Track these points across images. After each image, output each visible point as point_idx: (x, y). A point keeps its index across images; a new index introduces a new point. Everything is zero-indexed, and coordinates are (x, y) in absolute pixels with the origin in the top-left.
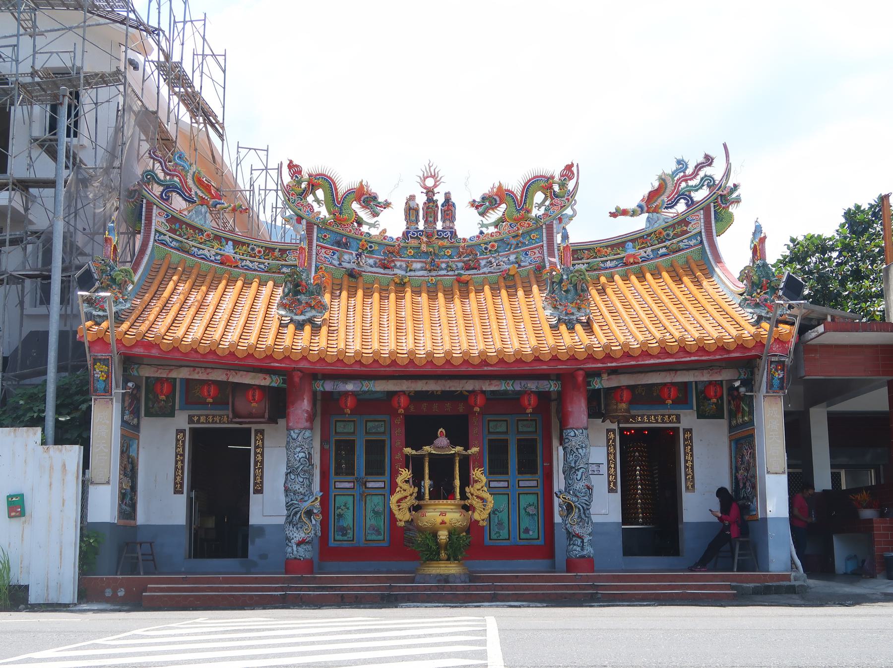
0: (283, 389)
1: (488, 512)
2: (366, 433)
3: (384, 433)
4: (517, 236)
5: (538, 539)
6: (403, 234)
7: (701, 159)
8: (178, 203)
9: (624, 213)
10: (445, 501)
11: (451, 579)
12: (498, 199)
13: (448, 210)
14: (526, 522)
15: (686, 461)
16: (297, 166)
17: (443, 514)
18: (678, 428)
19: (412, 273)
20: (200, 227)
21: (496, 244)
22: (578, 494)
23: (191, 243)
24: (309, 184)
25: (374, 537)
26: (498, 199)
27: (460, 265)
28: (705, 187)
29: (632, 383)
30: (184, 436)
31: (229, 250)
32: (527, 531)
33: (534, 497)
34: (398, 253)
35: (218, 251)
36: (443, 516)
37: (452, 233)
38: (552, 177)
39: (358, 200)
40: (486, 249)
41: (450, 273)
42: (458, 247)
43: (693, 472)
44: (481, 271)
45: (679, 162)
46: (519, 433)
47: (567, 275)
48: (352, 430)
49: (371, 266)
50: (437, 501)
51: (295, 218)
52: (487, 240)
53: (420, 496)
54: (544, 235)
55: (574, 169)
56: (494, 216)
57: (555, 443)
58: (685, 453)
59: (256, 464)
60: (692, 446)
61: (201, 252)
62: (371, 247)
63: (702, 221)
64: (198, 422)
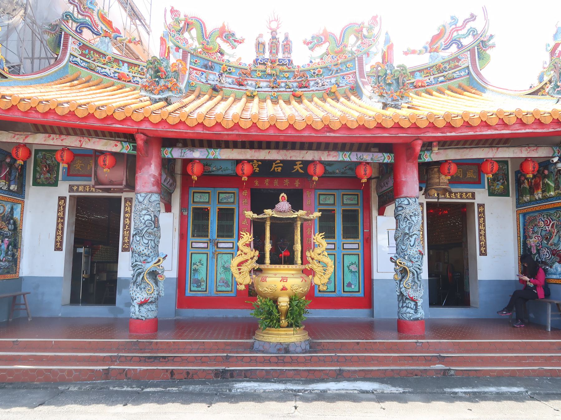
0: (134, 156)
1: (328, 276)
2: (219, 202)
3: (233, 203)
4: (337, 65)
5: (359, 292)
6: (254, 61)
7: (468, 16)
8: (87, 34)
9: (413, 52)
10: (286, 266)
11: (291, 349)
12: (323, 38)
13: (287, 44)
14: (349, 278)
15: (480, 230)
16: (177, 11)
17: (284, 279)
18: (473, 203)
19: (259, 89)
20: (103, 51)
21: (322, 70)
22: (413, 260)
23: (96, 64)
24: (185, 23)
25: (224, 289)
26: (323, 38)
27: (295, 84)
28: (470, 36)
29: (458, 157)
30: (65, 202)
31: (125, 69)
32: (349, 285)
33: (356, 257)
34: (250, 74)
35: (117, 70)
36: (282, 281)
37: (289, 60)
38: (363, 23)
39: (221, 36)
40: (314, 73)
41: (288, 90)
42: (294, 72)
43: (485, 239)
44: (310, 89)
45: (452, 18)
46: (344, 204)
47: (391, 70)
48: (207, 200)
49: (230, 84)
50: (278, 266)
51: (175, 47)
52: (314, 67)
53: (261, 260)
54: (357, 64)
55: (378, 19)
56: (321, 50)
57: (375, 213)
58: (480, 224)
59: (124, 227)
60: (484, 218)
61: (103, 70)
62: (230, 70)
63: (469, 59)
64: (77, 191)
